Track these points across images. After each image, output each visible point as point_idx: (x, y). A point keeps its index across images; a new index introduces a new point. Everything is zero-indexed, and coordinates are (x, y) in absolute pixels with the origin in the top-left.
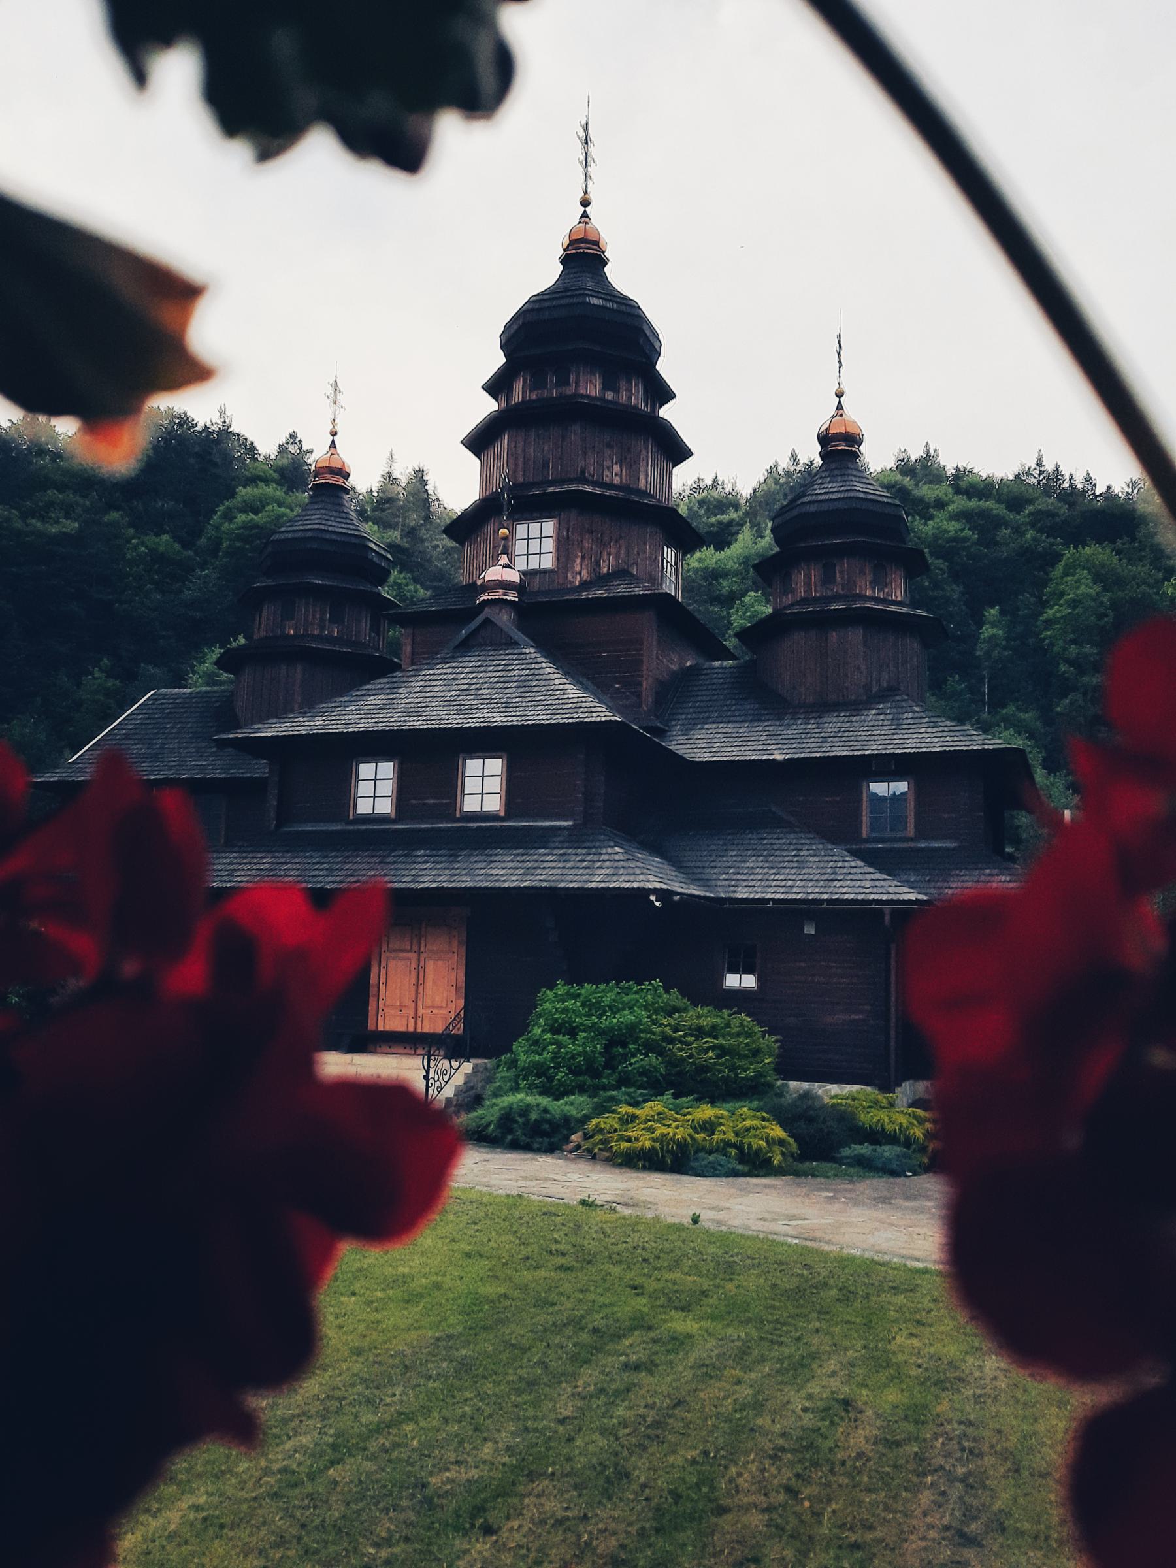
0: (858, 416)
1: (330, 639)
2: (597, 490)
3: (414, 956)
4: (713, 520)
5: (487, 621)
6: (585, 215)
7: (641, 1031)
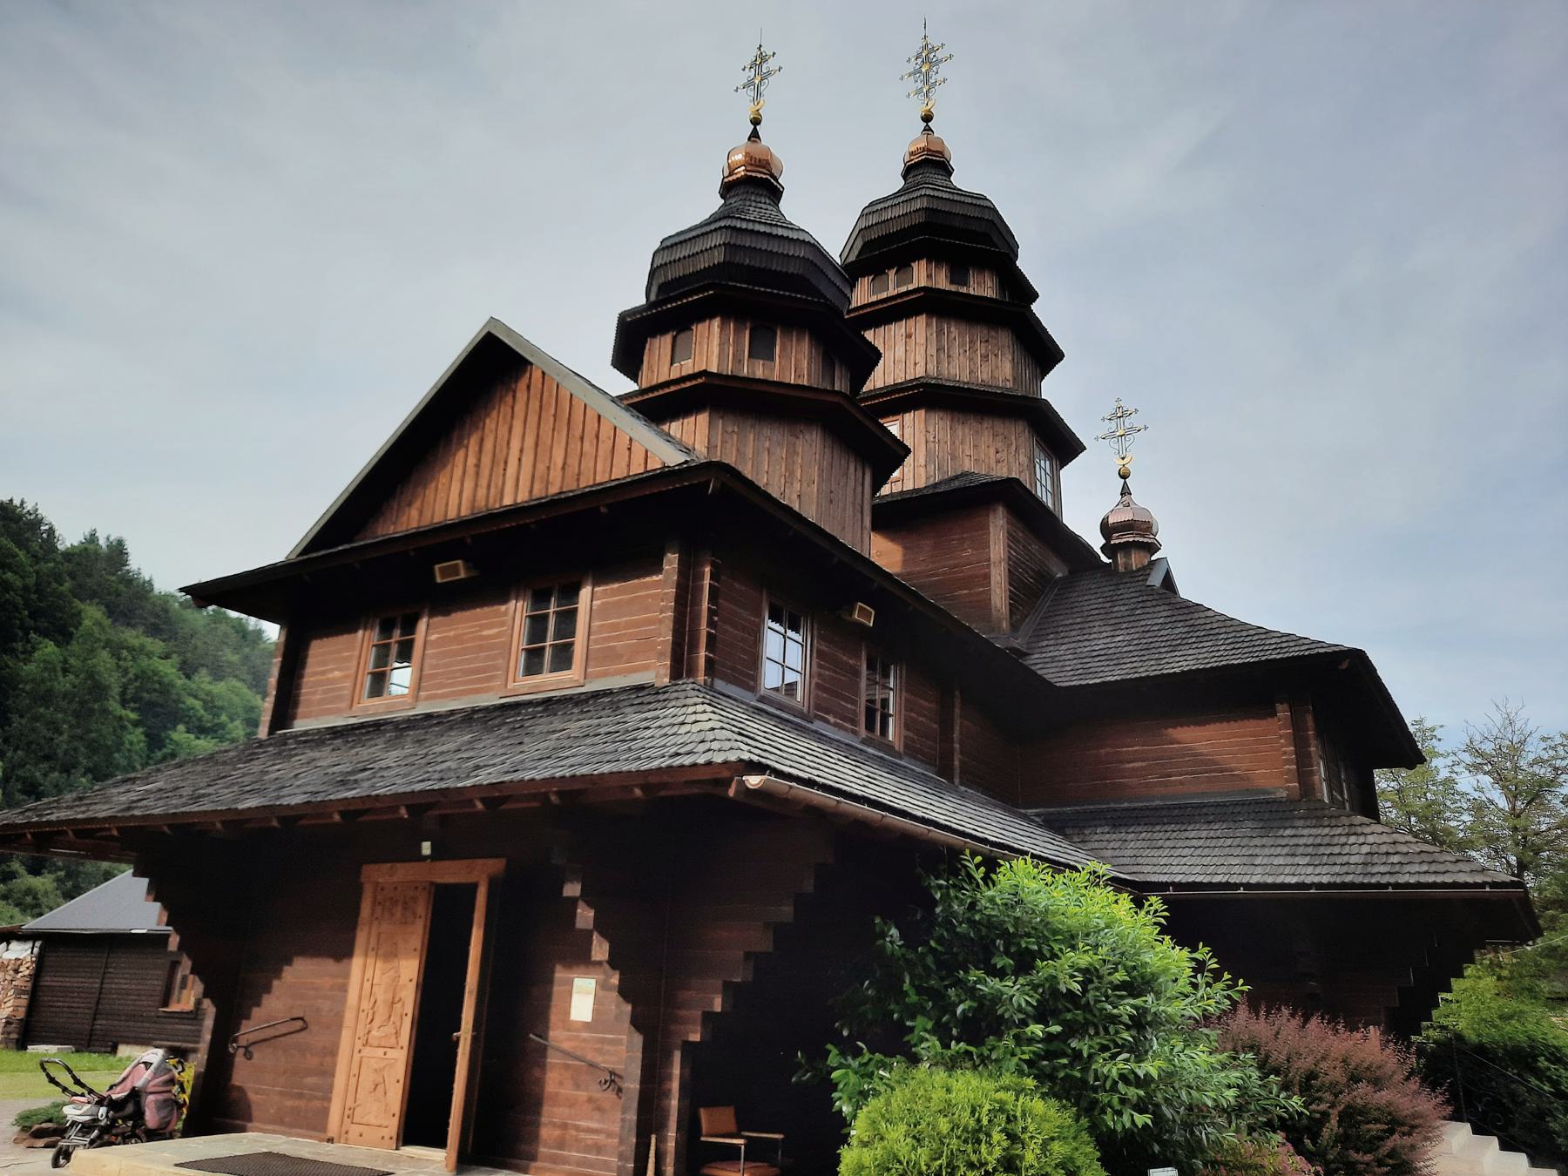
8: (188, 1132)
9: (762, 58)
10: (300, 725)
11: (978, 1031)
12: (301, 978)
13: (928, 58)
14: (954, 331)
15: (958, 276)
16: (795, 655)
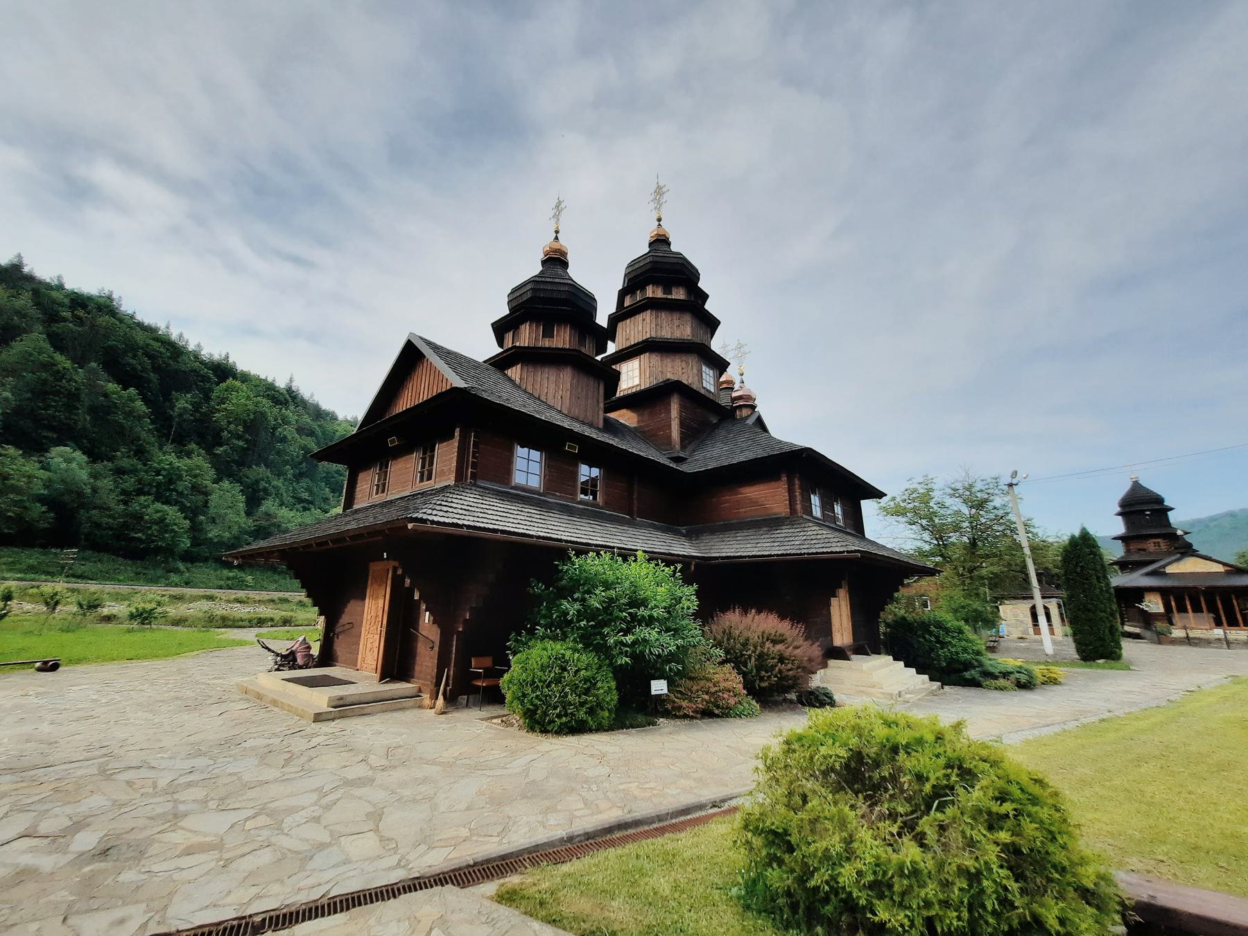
0: (564, 242)
8: (315, 667)
9: (560, 202)
10: (356, 507)
11: (561, 627)
12: (352, 606)
13: (659, 191)
14: (663, 315)
15: (667, 290)
16: (536, 468)
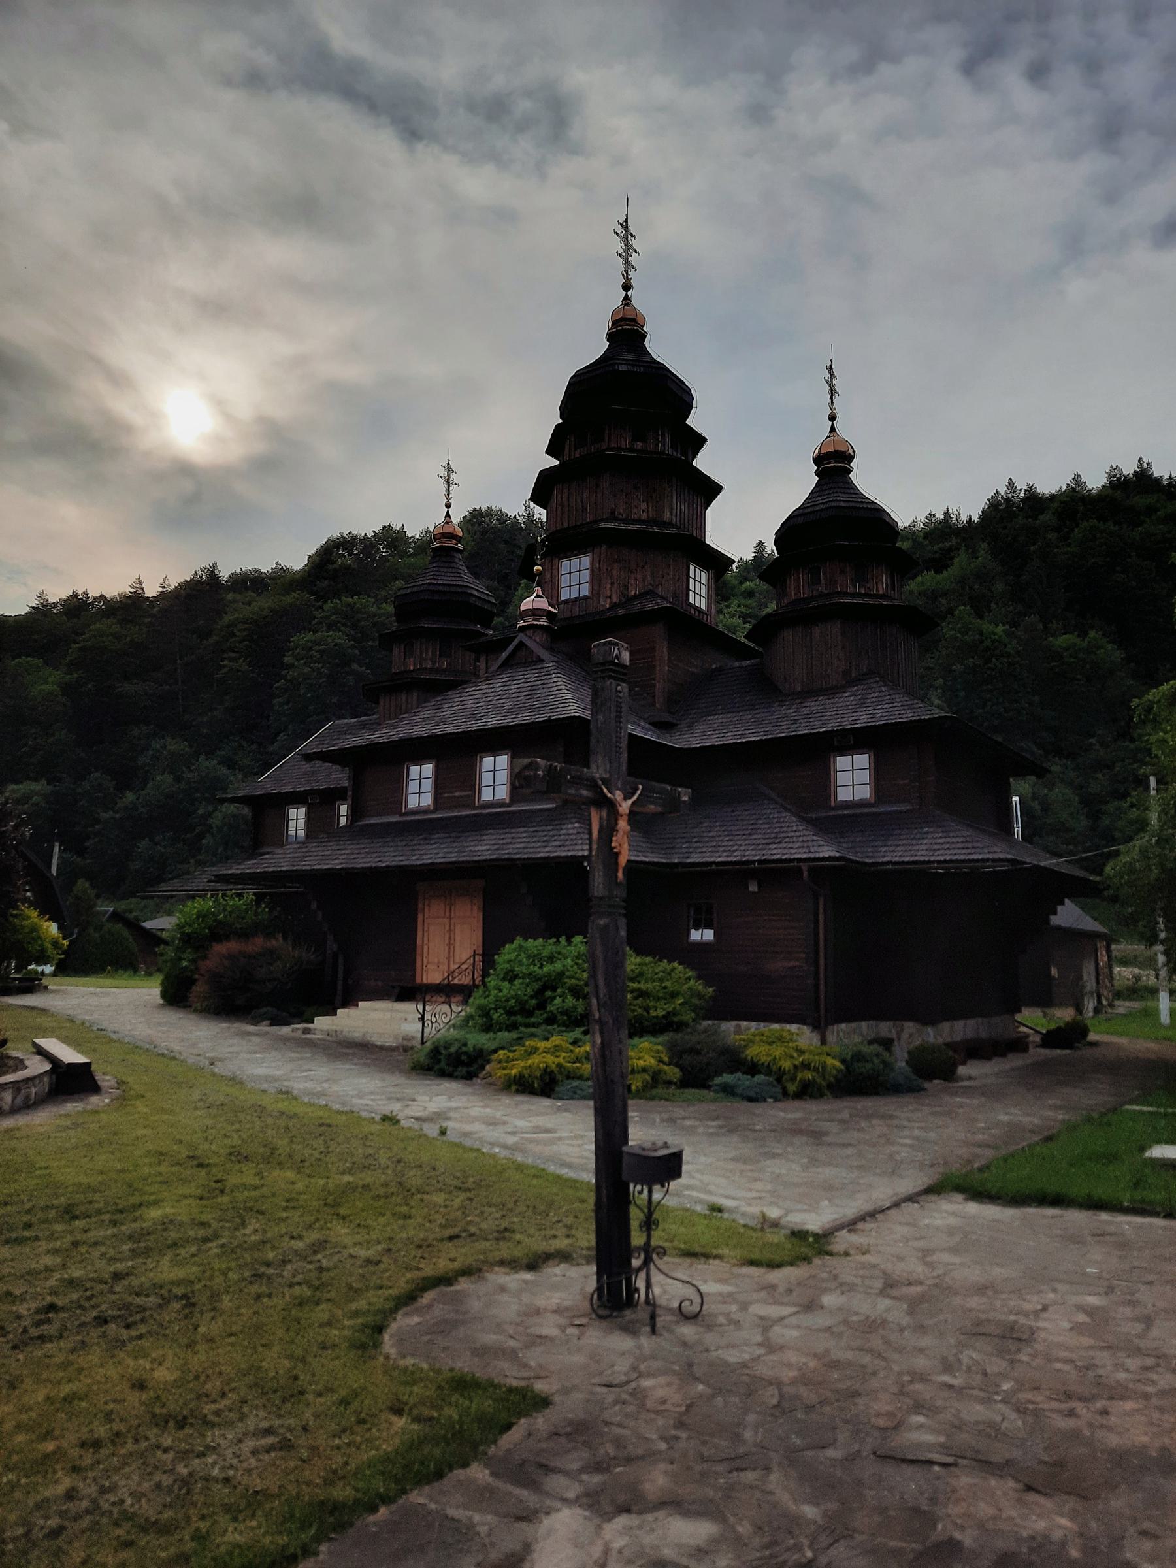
1: (438, 671)
2: (622, 526)
3: (446, 921)
4: (936, 547)
5: (521, 645)
6: (626, 298)
7: (568, 977)
